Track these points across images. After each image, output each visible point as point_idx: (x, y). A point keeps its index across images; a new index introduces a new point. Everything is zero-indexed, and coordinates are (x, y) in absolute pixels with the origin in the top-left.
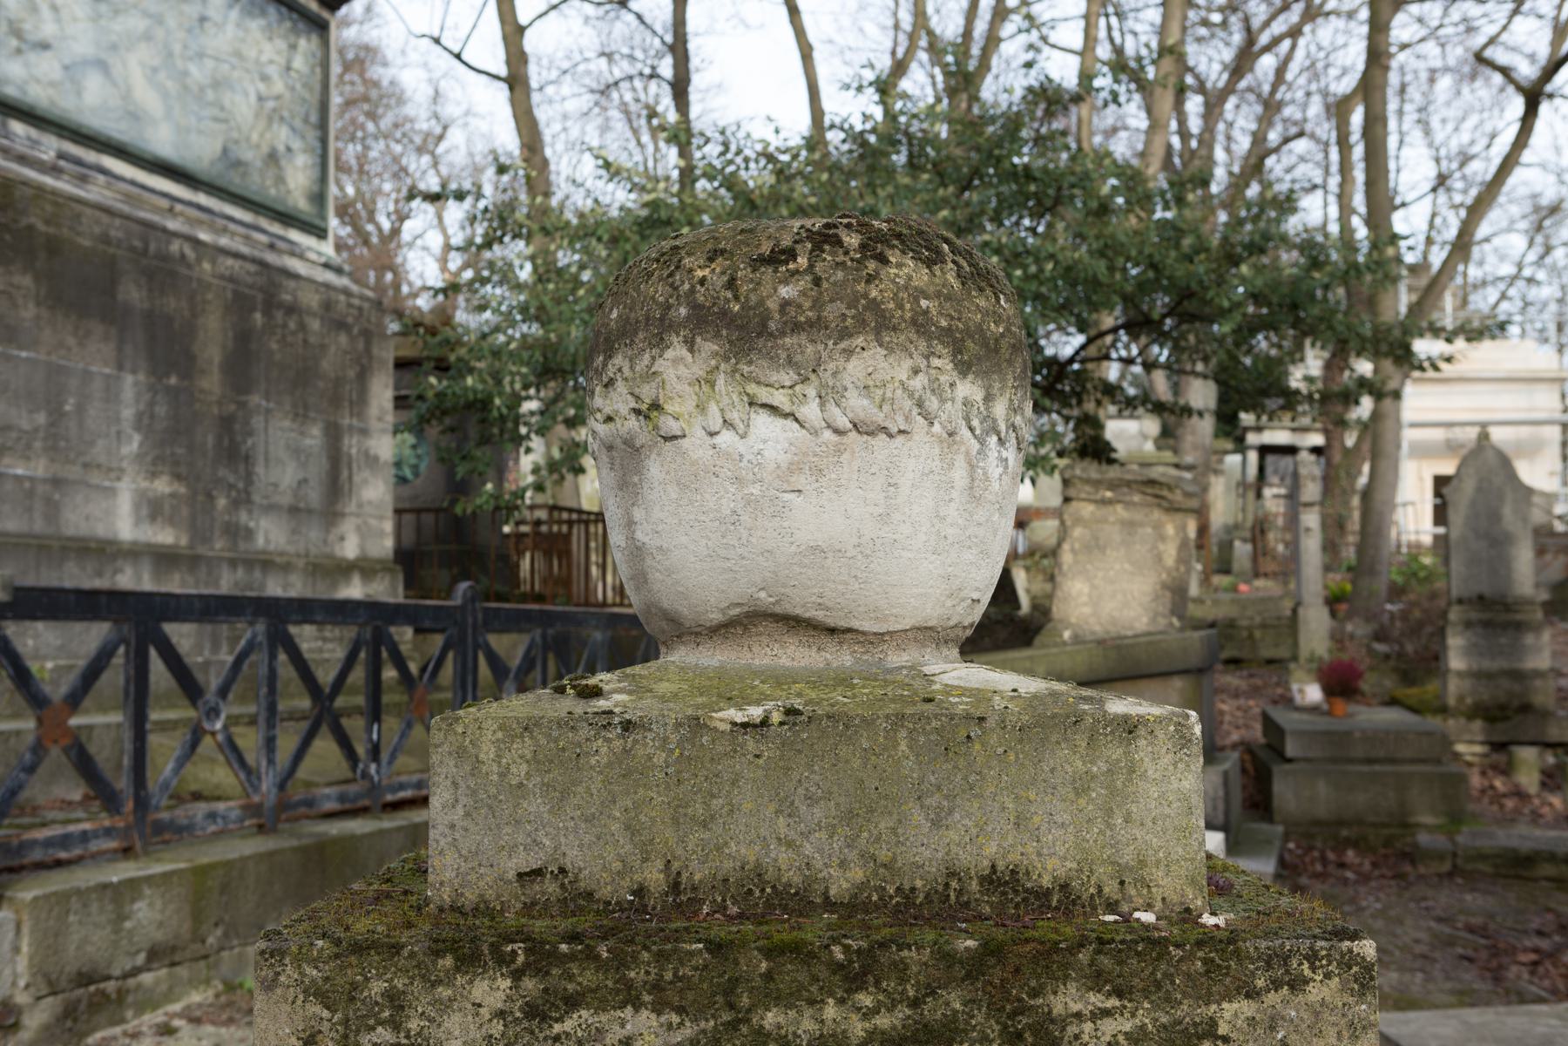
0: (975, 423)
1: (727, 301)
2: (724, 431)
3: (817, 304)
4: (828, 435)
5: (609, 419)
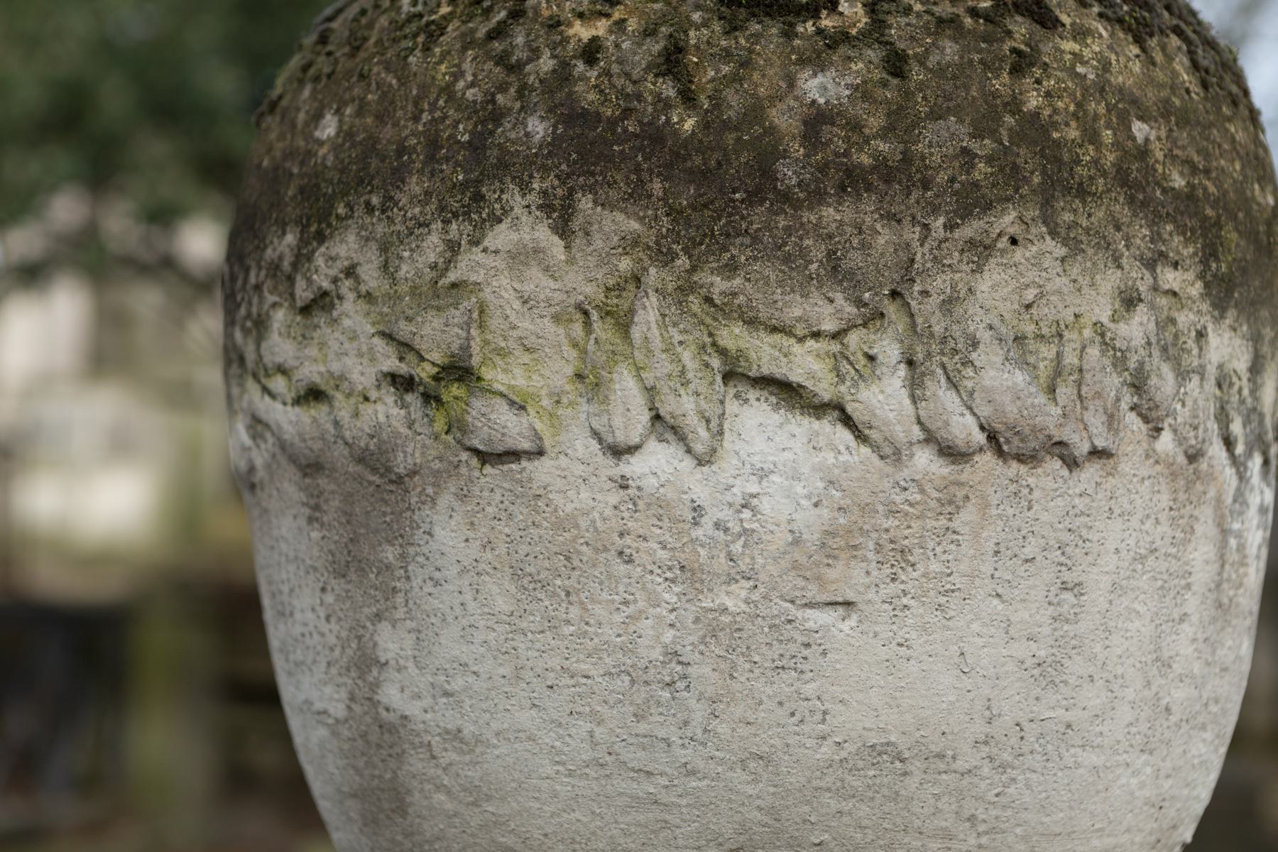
0: (1237, 428)
1: (664, 105)
2: (652, 445)
3: (900, 123)
4: (924, 460)
5: (314, 395)
